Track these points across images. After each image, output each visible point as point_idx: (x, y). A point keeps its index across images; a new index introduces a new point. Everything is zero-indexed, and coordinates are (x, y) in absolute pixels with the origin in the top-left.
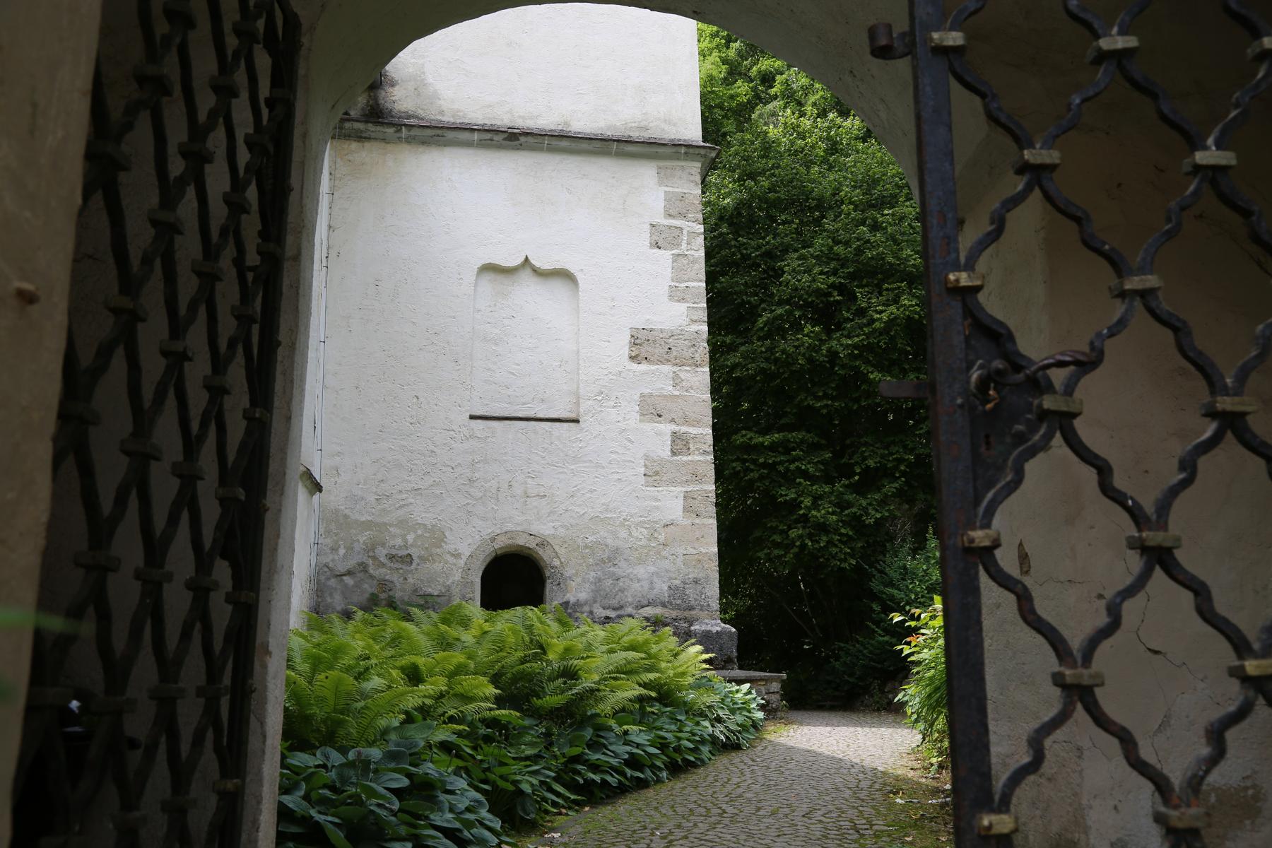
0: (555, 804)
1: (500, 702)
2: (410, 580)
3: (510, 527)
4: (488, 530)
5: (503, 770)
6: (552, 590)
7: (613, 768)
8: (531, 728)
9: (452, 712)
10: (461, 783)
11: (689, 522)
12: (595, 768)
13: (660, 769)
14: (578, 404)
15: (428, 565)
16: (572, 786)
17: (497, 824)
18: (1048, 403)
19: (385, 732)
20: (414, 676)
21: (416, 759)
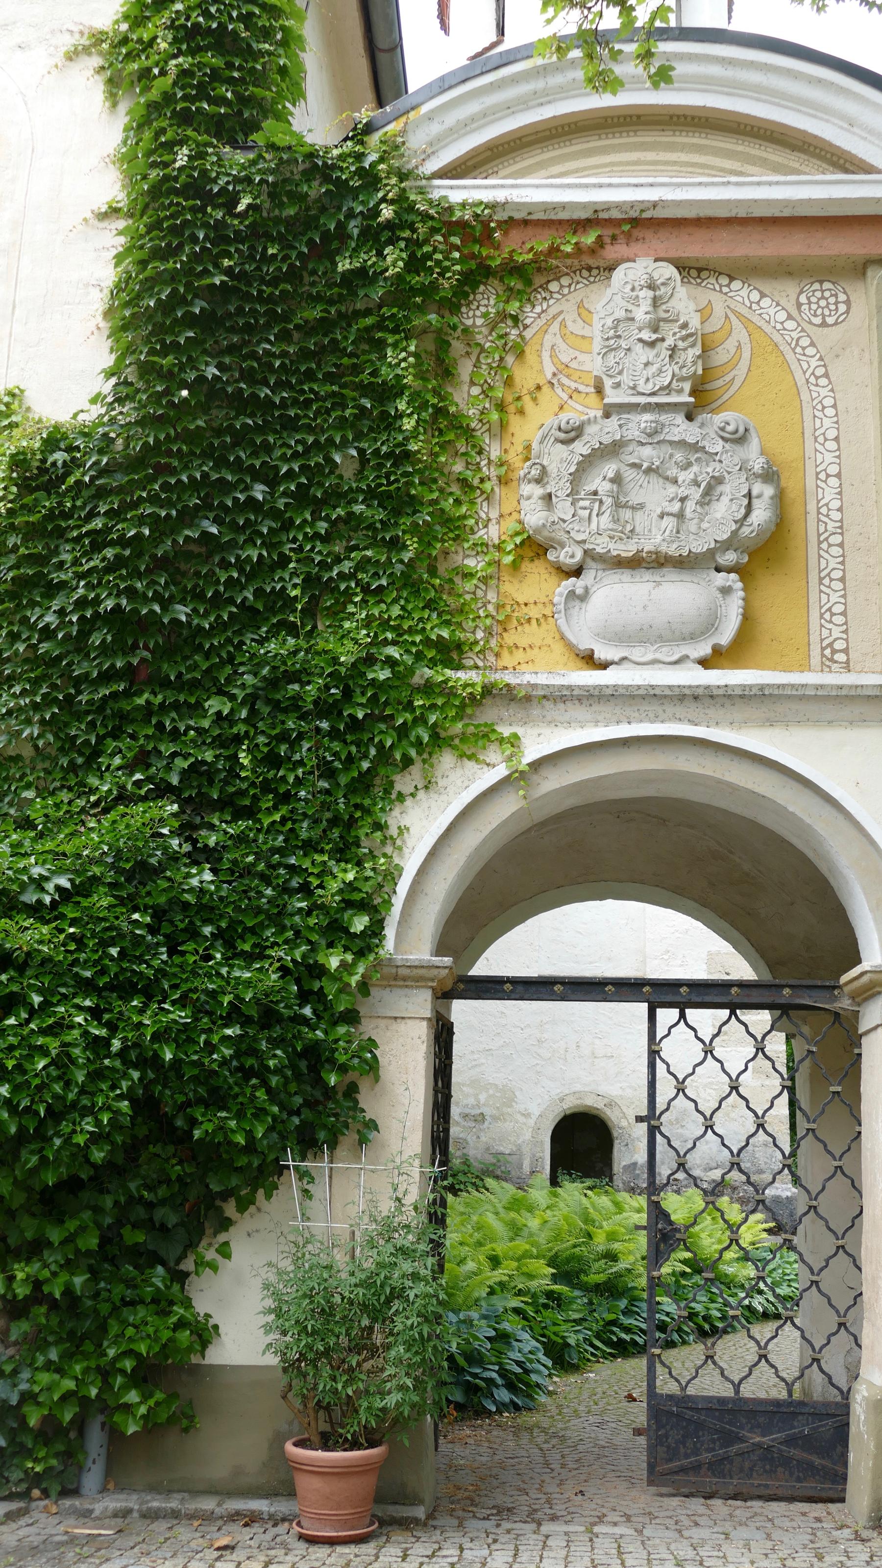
0: (592, 1354)
1: (555, 1278)
2: (483, 1139)
3: (578, 1087)
4: (557, 1090)
5: (556, 1329)
6: (620, 1151)
7: (641, 1330)
8: (576, 1298)
9: (520, 1286)
10: (526, 1336)
11: (759, 1083)
12: (627, 1330)
13: (687, 1334)
14: (644, 962)
15: (500, 1124)
16: (608, 1343)
17: (550, 1364)
18: (678, 1236)
19: (477, 1300)
20: (495, 1261)
21: (498, 1319)
